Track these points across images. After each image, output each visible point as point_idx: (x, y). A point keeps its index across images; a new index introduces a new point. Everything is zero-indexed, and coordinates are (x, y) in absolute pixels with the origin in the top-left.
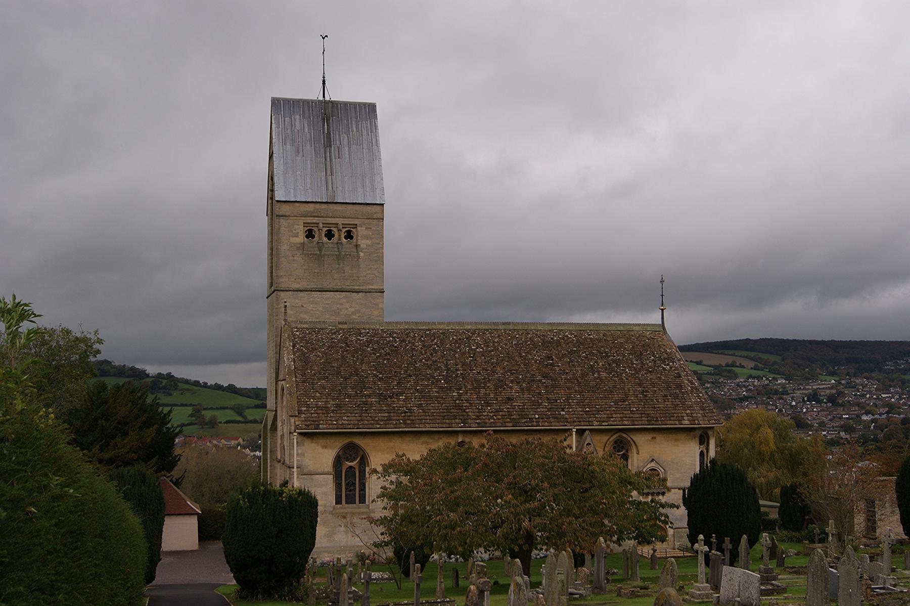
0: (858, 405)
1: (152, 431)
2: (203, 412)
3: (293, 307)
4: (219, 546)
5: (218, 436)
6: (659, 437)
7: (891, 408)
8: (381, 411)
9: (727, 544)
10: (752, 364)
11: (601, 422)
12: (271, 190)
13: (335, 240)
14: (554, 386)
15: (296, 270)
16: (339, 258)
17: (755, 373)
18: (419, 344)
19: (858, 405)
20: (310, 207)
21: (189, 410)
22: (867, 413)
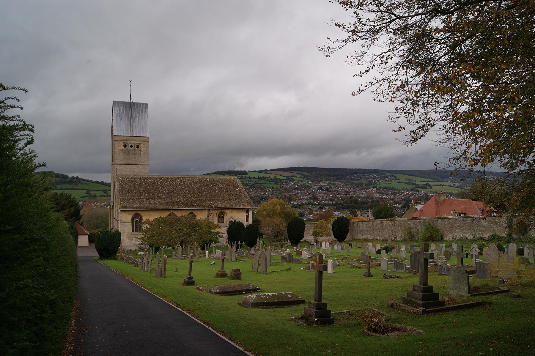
0: (336, 191)
1: (73, 209)
3: (119, 170)
4: (94, 245)
5: (97, 202)
6: (233, 211)
7: (347, 193)
8: (147, 203)
9: (231, 243)
10: (300, 176)
11: (215, 207)
13: (133, 148)
14: (201, 196)
15: (120, 158)
16: (134, 154)
17: (301, 179)
19: (336, 191)
21: (85, 191)
22: (338, 194)
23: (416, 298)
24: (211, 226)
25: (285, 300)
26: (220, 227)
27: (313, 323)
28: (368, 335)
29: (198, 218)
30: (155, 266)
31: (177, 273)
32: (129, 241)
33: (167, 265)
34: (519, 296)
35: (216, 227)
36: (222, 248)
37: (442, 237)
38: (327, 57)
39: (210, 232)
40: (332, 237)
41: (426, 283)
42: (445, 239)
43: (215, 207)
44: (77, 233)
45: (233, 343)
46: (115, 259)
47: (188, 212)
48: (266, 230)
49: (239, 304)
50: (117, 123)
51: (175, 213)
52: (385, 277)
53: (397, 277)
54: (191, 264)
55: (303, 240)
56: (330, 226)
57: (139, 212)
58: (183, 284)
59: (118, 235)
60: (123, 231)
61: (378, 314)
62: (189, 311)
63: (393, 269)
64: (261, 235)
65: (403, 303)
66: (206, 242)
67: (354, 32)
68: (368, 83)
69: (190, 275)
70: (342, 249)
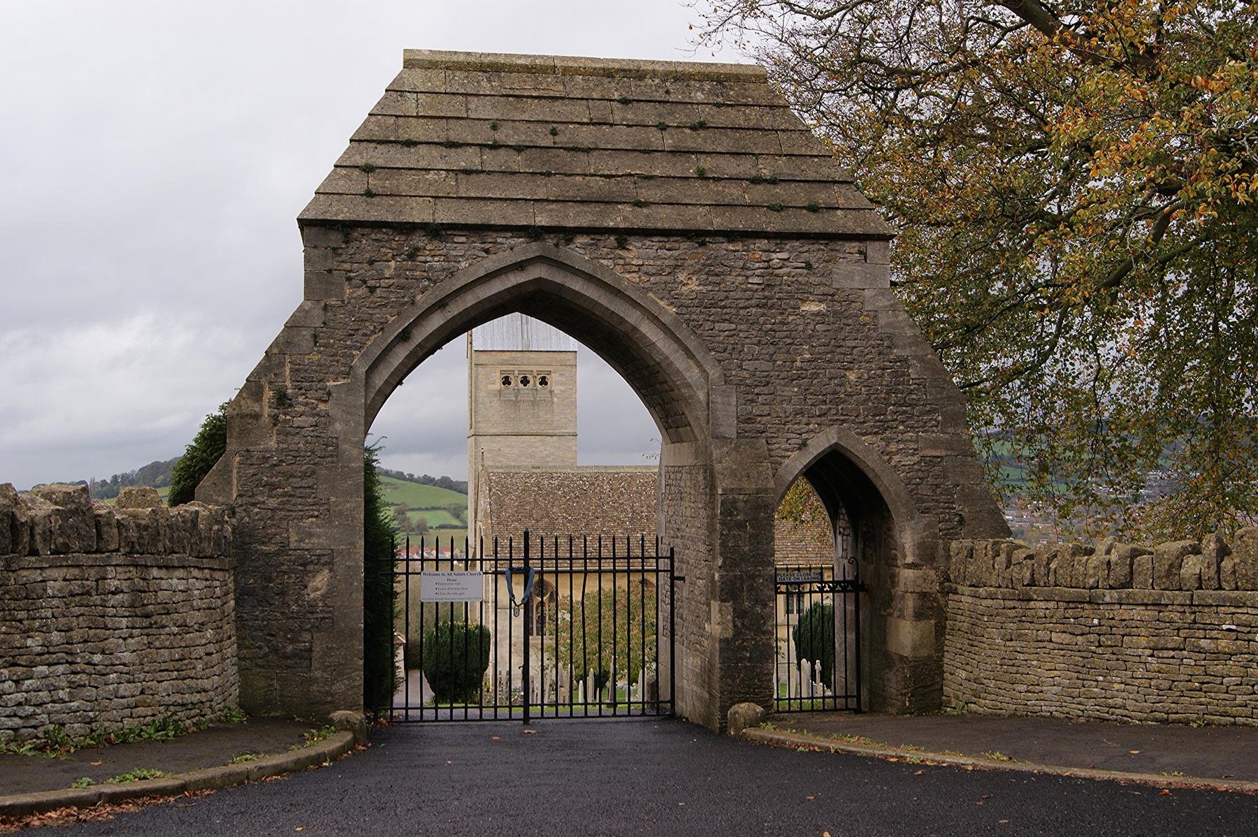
2: (409, 514)
16: (534, 403)
18: (607, 487)
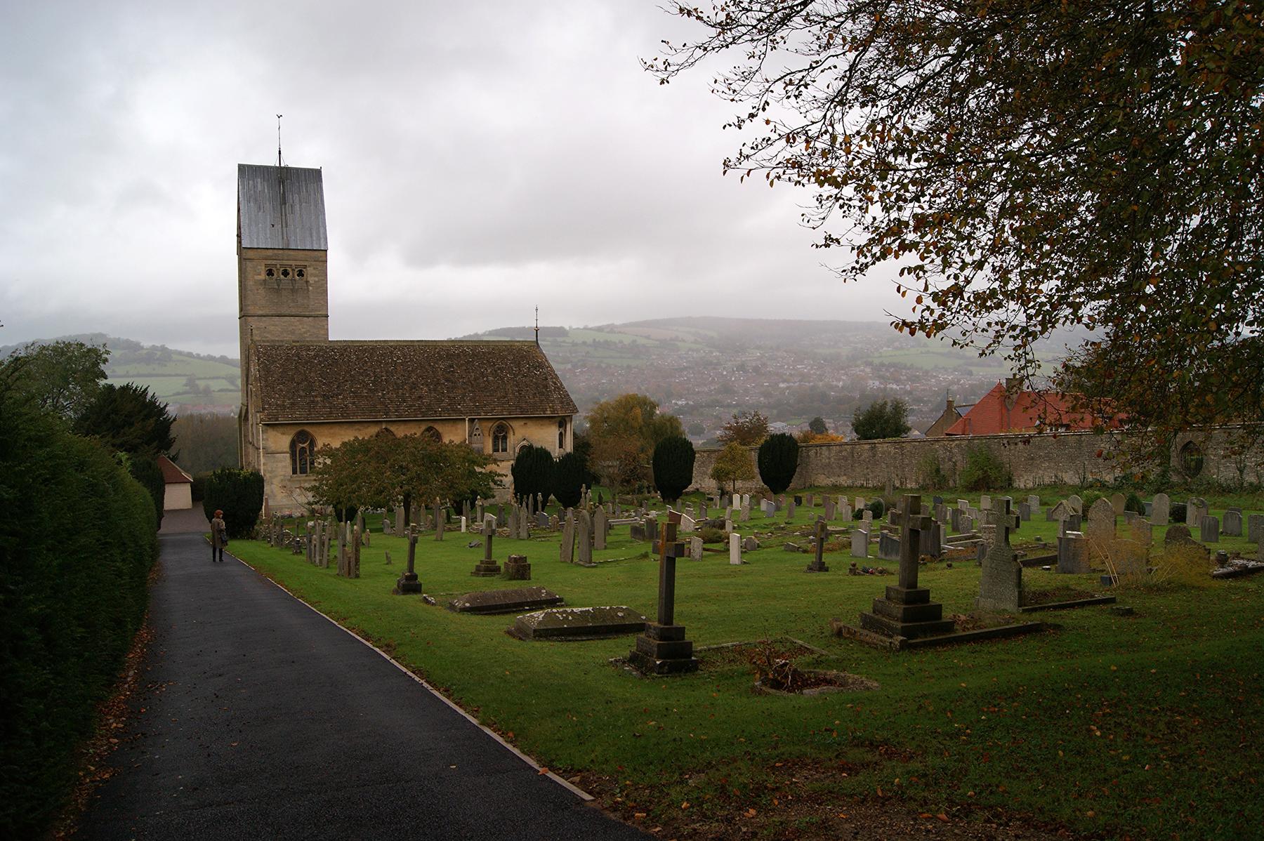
2: (197, 382)
3: (258, 328)
6: (530, 423)
11: (486, 413)
12: (239, 242)
13: (290, 277)
16: (293, 291)
20: (270, 253)
21: (183, 380)
22: (784, 381)
23: (889, 615)
24: (472, 457)
25: (609, 623)
26: (495, 461)
27: (652, 670)
28: (760, 693)
29: (446, 440)
30: (335, 552)
31: (390, 568)
32: (284, 493)
33: (362, 550)
34: (1129, 612)
35: (488, 460)
36: (499, 510)
37: (1010, 481)
38: (662, 82)
39: (472, 474)
40: (758, 483)
41: (913, 584)
42: (1015, 485)
43: (486, 413)
44: (162, 479)
45: (461, 711)
46: (251, 536)
47: (424, 427)
48: (608, 466)
49: (509, 633)
50: (250, 219)
51: (393, 428)
52: (853, 571)
53: (881, 572)
54: (413, 546)
55: (690, 488)
56: (754, 456)
57: (308, 429)
58: (396, 592)
59: (256, 483)
60: (271, 472)
61: (802, 650)
62: (388, 648)
63: (879, 554)
64: (593, 480)
65: (864, 627)
66: (465, 495)
67: (724, 27)
68: (760, 140)
69: (411, 568)
70: (778, 509)
